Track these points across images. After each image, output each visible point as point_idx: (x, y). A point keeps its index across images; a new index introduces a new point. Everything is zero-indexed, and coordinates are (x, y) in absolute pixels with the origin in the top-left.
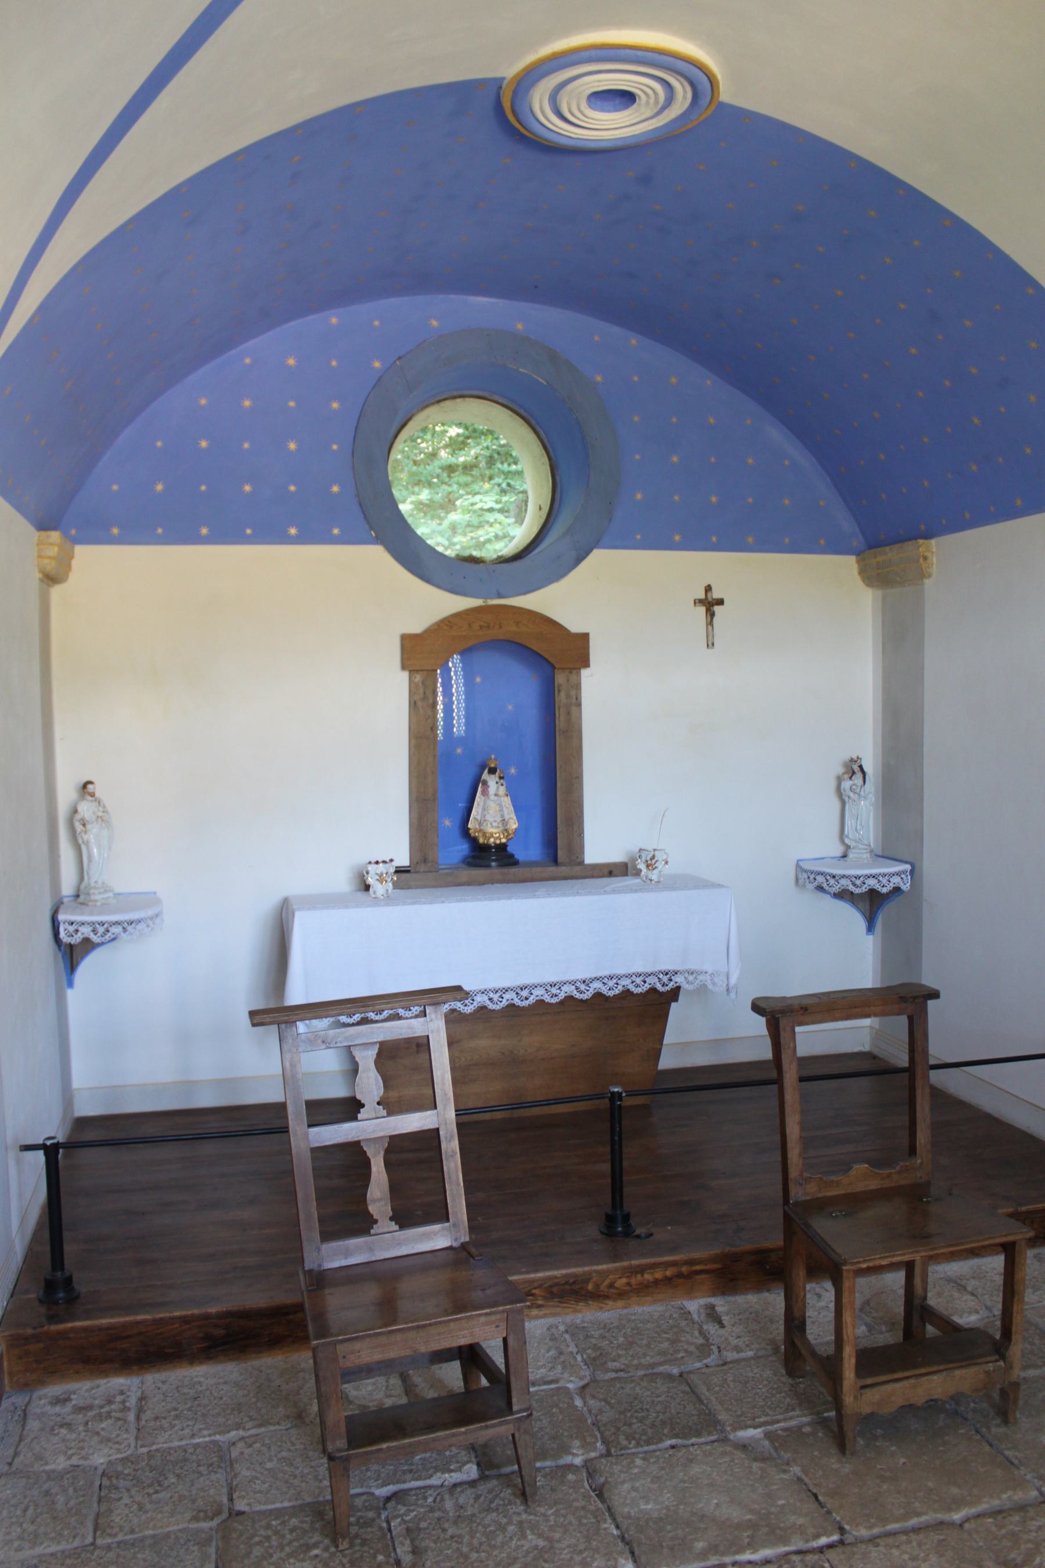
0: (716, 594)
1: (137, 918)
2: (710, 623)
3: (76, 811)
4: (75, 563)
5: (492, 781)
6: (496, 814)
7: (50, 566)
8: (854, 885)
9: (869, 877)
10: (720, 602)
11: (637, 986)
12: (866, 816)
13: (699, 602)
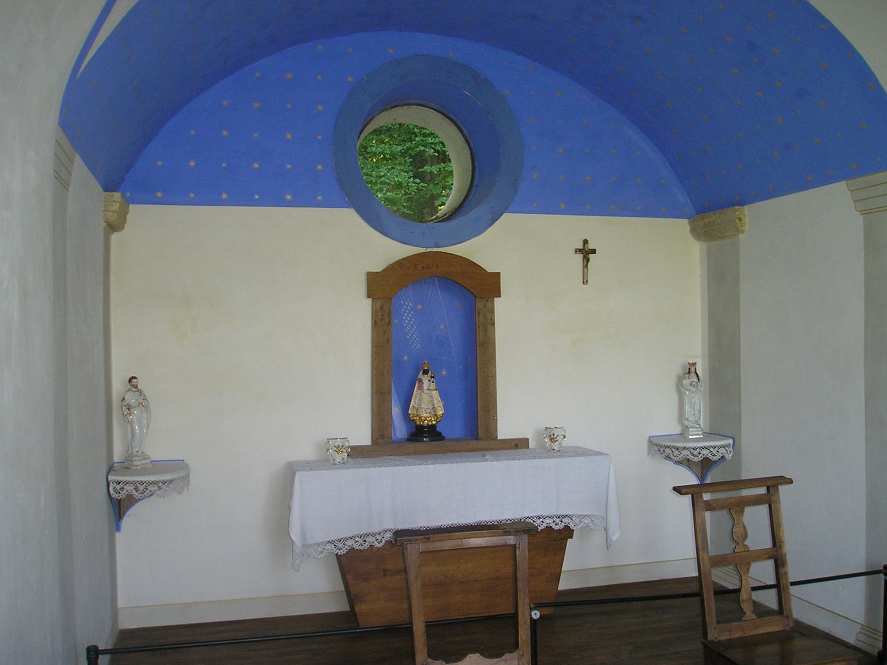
0: (591, 246)
1: (173, 476)
2: (586, 266)
3: (124, 399)
4: (128, 217)
5: (426, 380)
6: (428, 403)
7: (113, 218)
8: (693, 455)
9: (702, 448)
10: (594, 251)
11: (557, 524)
12: (698, 404)
13: (578, 251)
